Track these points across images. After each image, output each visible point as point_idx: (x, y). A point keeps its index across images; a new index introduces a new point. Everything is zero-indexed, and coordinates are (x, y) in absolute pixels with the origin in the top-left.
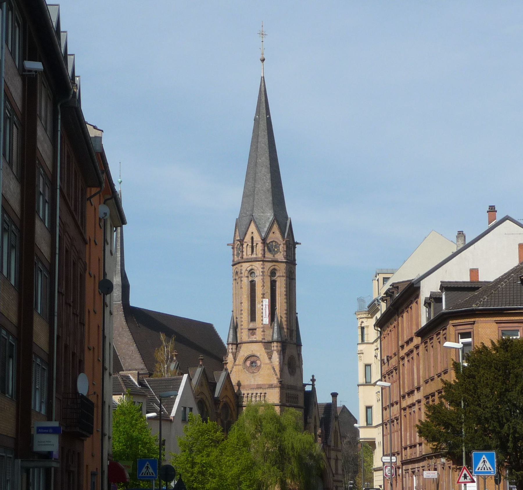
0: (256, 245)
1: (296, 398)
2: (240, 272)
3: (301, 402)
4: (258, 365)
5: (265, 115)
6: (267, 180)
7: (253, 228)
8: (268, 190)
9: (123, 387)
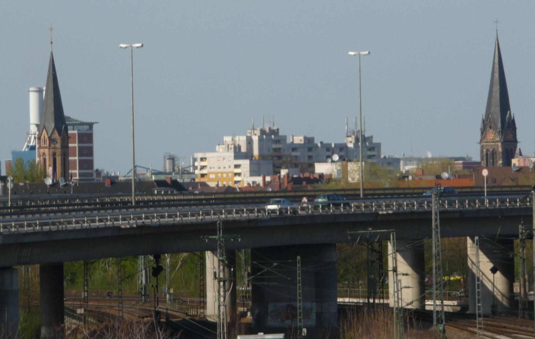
7: (44, 132)
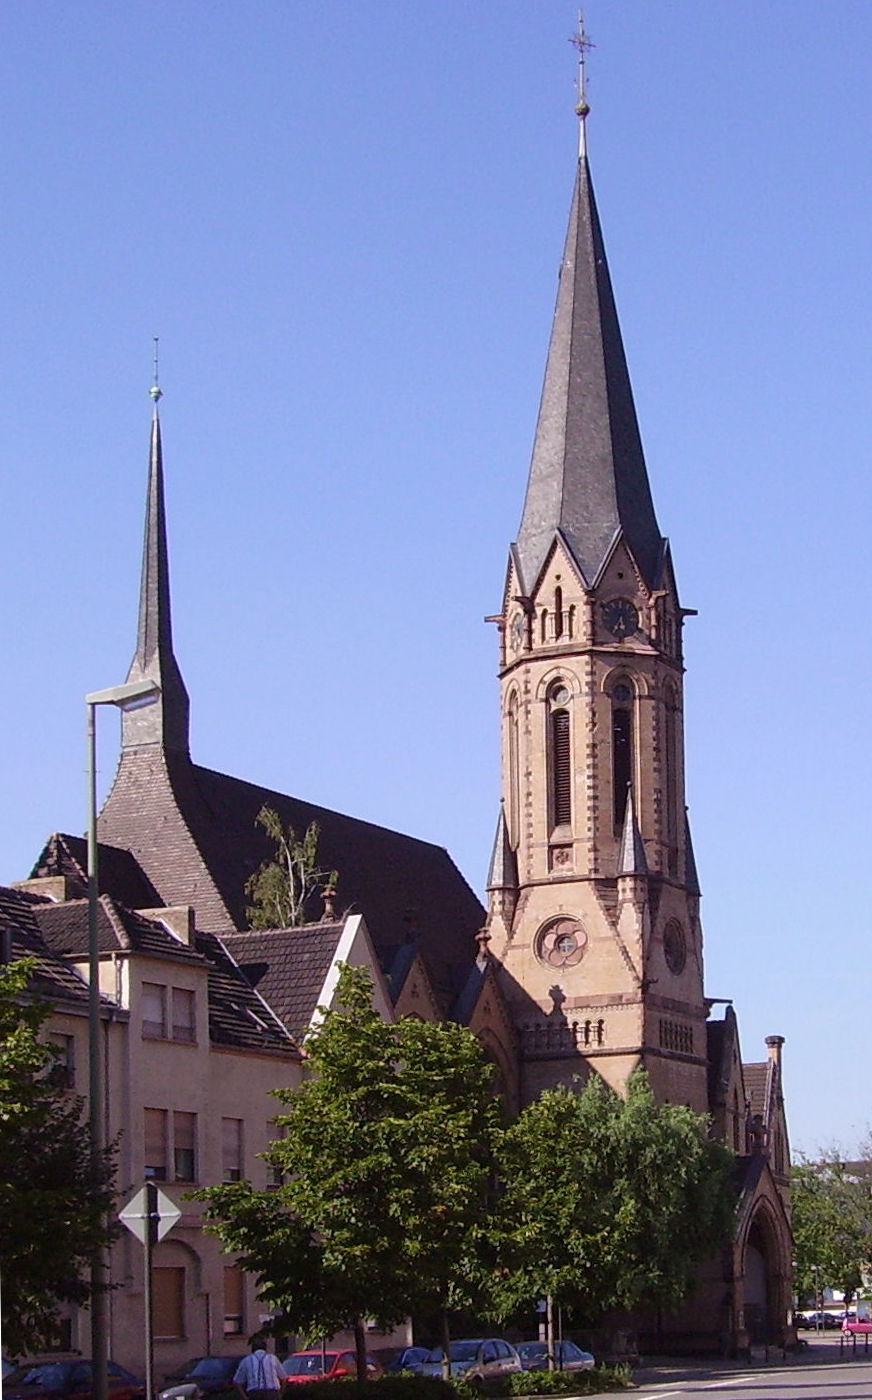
0: (568, 609)
1: (688, 1036)
2: (523, 689)
3: (700, 1048)
4: (580, 944)
5: (591, 259)
6: (598, 433)
8: (604, 460)
9: (118, 935)
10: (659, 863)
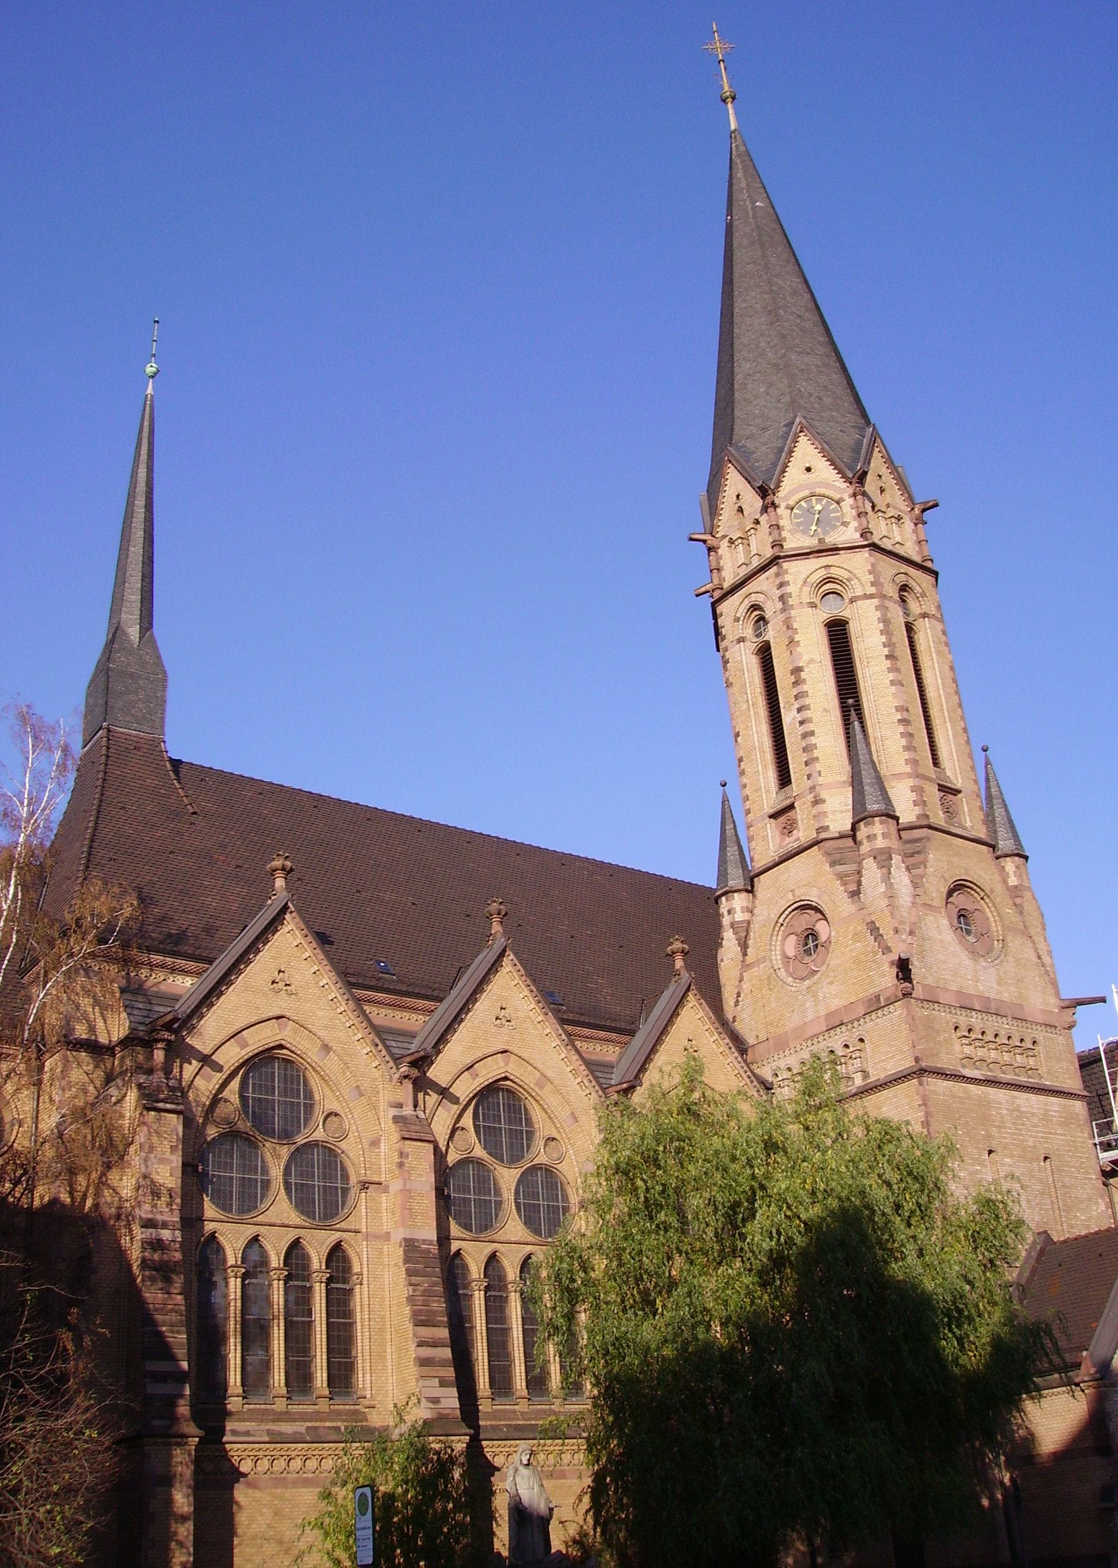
10: (921, 802)
